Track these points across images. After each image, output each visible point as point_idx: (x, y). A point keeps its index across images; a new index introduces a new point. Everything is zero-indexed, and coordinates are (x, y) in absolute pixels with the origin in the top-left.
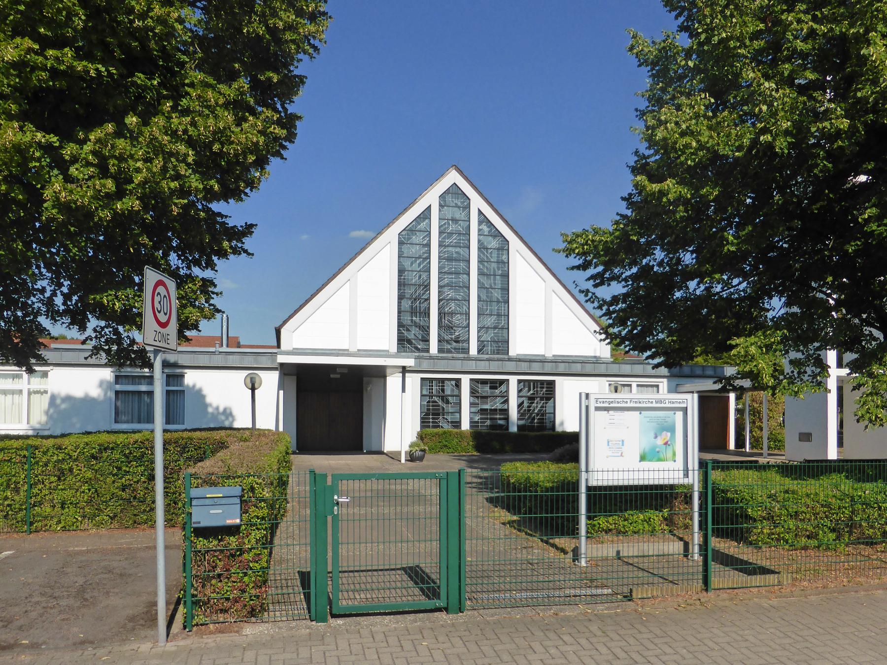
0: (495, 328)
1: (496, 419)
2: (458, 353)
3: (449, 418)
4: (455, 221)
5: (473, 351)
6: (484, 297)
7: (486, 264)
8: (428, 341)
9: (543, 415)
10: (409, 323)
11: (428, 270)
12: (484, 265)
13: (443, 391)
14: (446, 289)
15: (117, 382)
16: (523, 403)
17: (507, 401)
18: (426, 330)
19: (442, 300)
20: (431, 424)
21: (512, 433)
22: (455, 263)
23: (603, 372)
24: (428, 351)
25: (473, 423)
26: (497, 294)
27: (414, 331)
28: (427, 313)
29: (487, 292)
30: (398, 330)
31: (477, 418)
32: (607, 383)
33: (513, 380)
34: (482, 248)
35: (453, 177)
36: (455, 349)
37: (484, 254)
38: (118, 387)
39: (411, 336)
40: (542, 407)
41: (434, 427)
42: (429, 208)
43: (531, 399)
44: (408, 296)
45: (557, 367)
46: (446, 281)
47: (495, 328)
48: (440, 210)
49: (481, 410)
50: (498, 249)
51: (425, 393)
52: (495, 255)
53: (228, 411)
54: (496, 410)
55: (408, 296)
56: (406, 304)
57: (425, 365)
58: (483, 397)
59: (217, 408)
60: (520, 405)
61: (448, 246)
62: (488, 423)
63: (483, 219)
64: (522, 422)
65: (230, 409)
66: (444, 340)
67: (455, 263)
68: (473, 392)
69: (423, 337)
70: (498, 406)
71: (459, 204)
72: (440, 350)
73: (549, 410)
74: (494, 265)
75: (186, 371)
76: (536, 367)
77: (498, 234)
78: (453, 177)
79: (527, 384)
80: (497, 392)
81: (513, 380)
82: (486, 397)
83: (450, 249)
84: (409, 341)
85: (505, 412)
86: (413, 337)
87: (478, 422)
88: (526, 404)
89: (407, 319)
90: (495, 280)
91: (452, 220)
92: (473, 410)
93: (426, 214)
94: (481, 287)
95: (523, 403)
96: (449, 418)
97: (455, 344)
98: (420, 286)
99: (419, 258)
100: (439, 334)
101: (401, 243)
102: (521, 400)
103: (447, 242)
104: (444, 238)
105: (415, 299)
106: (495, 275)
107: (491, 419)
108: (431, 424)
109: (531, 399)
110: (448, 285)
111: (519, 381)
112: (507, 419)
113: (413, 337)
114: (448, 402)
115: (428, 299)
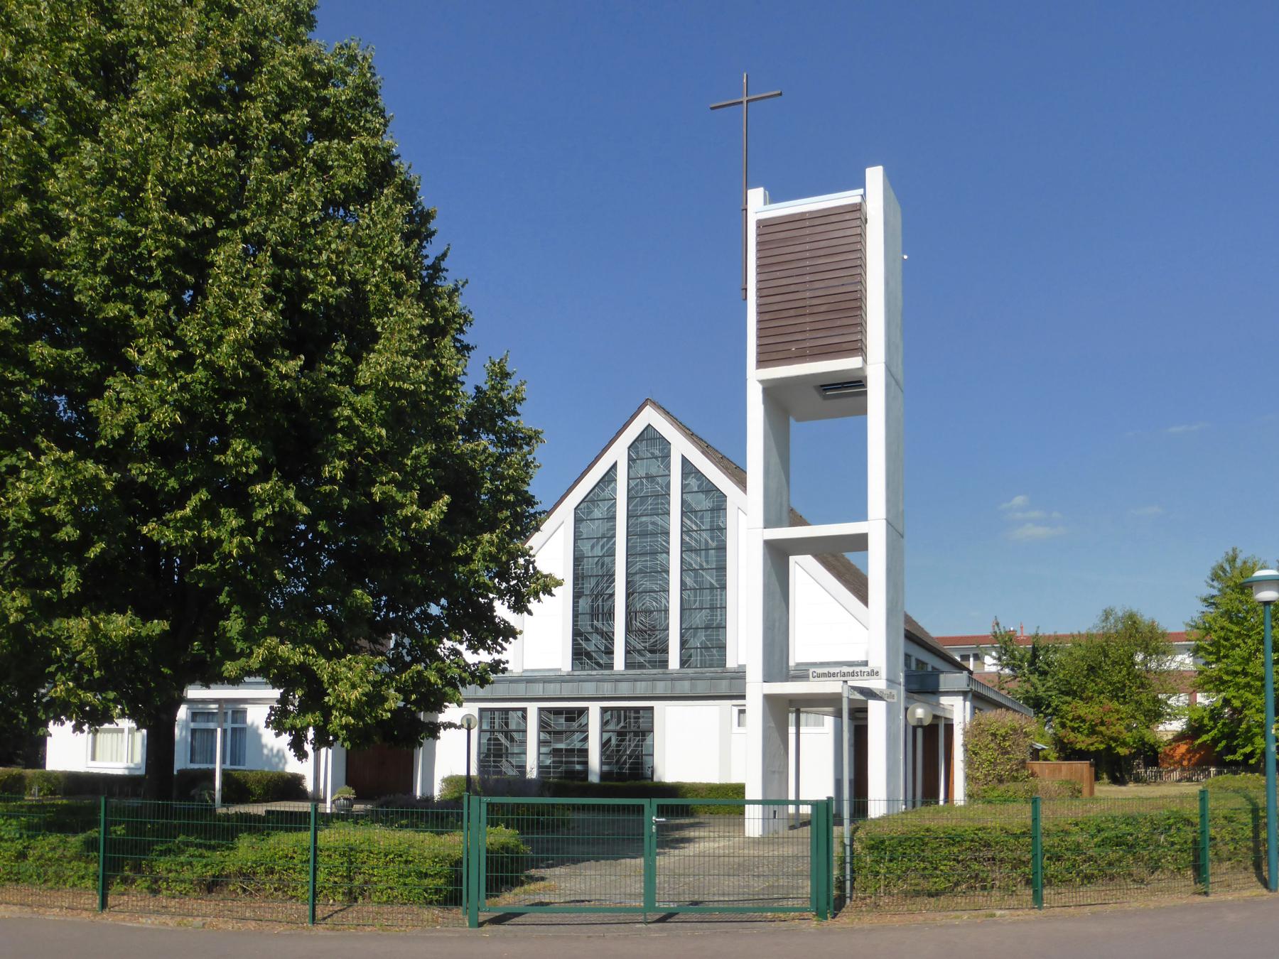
0: (707, 628)
1: (573, 763)
2: (654, 667)
4: (650, 478)
6: (689, 582)
7: (694, 534)
8: (612, 653)
9: (637, 757)
11: (612, 553)
12: (691, 537)
14: (637, 577)
15: (193, 720)
16: (609, 740)
17: (586, 739)
18: (609, 637)
21: (531, 781)
22: (647, 542)
23: (688, 692)
24: (611, 666)
25: (541, 767)
26: (710, 578)
27: (596, 639)
28: (610, 615)
30: (574, 640)
31: (548, 762)
33: (594, 709)
34: (686, 510)
35: (649, 416)
37: (691, 520)
38: (192, 725)
40: (636, 746)
41: (495, 773)
42: (614, 466)
43: (621, 734)
44: (587, 592)
45: (654, 688)
46: (638, 566)
47: (707, 628)
50: (712, 510)
51: (485, 727)
52: (707, 519)
54: (573, 750)
56: (584, 603)
57: (607, 689)
58: (557, 733)
59: (272, 750)
60: (605, 745)
61: (642, 515)
62: (563, 768)
63: (688, 468)
64: (606, 768)
66: (635, 650)
67: (647, 542)
68: (543, 726)
69: (606, 647)
70: (578, 745)
71: (657, 453)
72: (628, 665)
77: (710, 489)
78: (649, 416)
80: (575, 725)
81: (594, 709)
82: (560, 733)
83: (644, 519)
85: (584, 752)
86: (593, 648)
87: (548, 767)
88: (613, 742)
89: (586, 626)
90: (707, 556)
91: (647, 478)
92: (543, 750)
93: (609, 477)
95: (609, 740)
96: (514, 761)
97: (649, 655)
98: (603, 576)
100: (626, 642)
101: (578, 521)
102: (606, 736)
104: (636, 505)
106: (707, 549)
107: (567, 763)
109: (621, 734)
110: (641, 571)
111: (604, 710)
112: (586, 763)
113: (593, 648)
114: (512, 740)
115: (612, 595)
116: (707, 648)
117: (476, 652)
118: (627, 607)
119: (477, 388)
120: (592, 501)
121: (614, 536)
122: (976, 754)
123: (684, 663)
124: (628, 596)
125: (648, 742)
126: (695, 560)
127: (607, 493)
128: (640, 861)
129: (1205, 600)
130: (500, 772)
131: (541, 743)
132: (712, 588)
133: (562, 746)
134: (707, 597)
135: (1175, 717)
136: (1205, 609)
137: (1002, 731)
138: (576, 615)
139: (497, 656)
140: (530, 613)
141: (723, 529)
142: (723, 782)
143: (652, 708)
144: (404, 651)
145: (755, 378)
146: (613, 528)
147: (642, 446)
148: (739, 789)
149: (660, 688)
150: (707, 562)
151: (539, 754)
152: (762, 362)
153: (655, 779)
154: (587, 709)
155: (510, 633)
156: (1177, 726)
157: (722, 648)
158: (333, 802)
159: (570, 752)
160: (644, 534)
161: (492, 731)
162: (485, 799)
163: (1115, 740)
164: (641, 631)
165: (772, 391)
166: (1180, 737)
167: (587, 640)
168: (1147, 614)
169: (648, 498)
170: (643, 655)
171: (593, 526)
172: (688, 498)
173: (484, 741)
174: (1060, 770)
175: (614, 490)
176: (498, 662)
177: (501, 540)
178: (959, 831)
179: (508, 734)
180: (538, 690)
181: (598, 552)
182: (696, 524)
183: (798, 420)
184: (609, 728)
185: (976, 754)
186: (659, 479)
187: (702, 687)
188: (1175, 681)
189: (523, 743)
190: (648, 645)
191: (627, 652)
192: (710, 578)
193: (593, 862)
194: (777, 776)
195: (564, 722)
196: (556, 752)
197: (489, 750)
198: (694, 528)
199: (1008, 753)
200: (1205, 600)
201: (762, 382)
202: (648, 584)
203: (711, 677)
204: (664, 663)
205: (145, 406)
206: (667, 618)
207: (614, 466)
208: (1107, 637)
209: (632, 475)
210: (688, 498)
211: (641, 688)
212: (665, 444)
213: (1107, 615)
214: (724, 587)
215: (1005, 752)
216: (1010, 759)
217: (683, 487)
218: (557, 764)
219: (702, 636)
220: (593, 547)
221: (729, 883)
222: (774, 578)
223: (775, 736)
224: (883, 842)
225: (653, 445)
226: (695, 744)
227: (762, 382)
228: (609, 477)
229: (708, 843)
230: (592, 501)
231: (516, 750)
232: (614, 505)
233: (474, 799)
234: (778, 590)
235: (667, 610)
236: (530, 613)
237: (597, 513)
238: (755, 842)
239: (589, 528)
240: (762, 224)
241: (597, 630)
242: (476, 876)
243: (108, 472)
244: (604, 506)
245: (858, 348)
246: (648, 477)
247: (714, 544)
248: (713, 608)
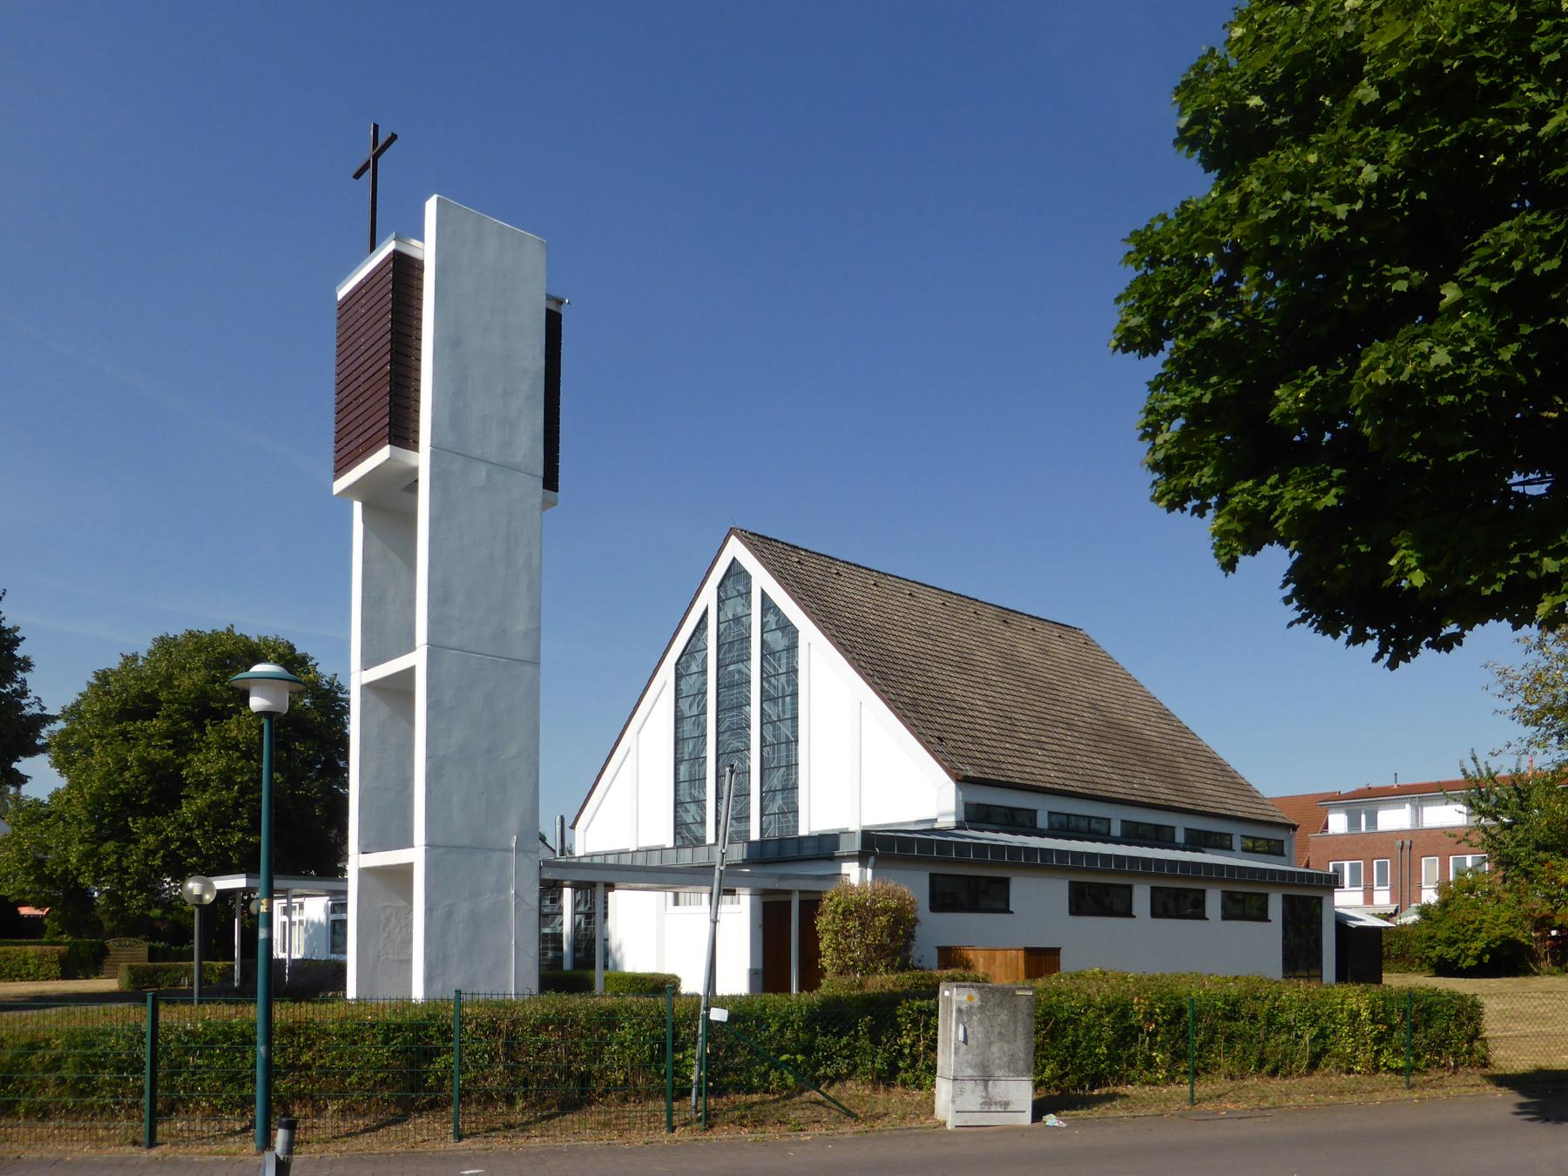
27: (693, 808)
47: (783, 790)
63: (767, 604)
101: (678, 677)
116: (784, 813)
121: (705, 693)
145: (418, 659)
146: (705, 683)
169: (733, 645)
205: (238, 743)
214: (797, 741)
223: (650, 986)
237: (694, 668)
239: (689, 685)
243: (1512, 214)
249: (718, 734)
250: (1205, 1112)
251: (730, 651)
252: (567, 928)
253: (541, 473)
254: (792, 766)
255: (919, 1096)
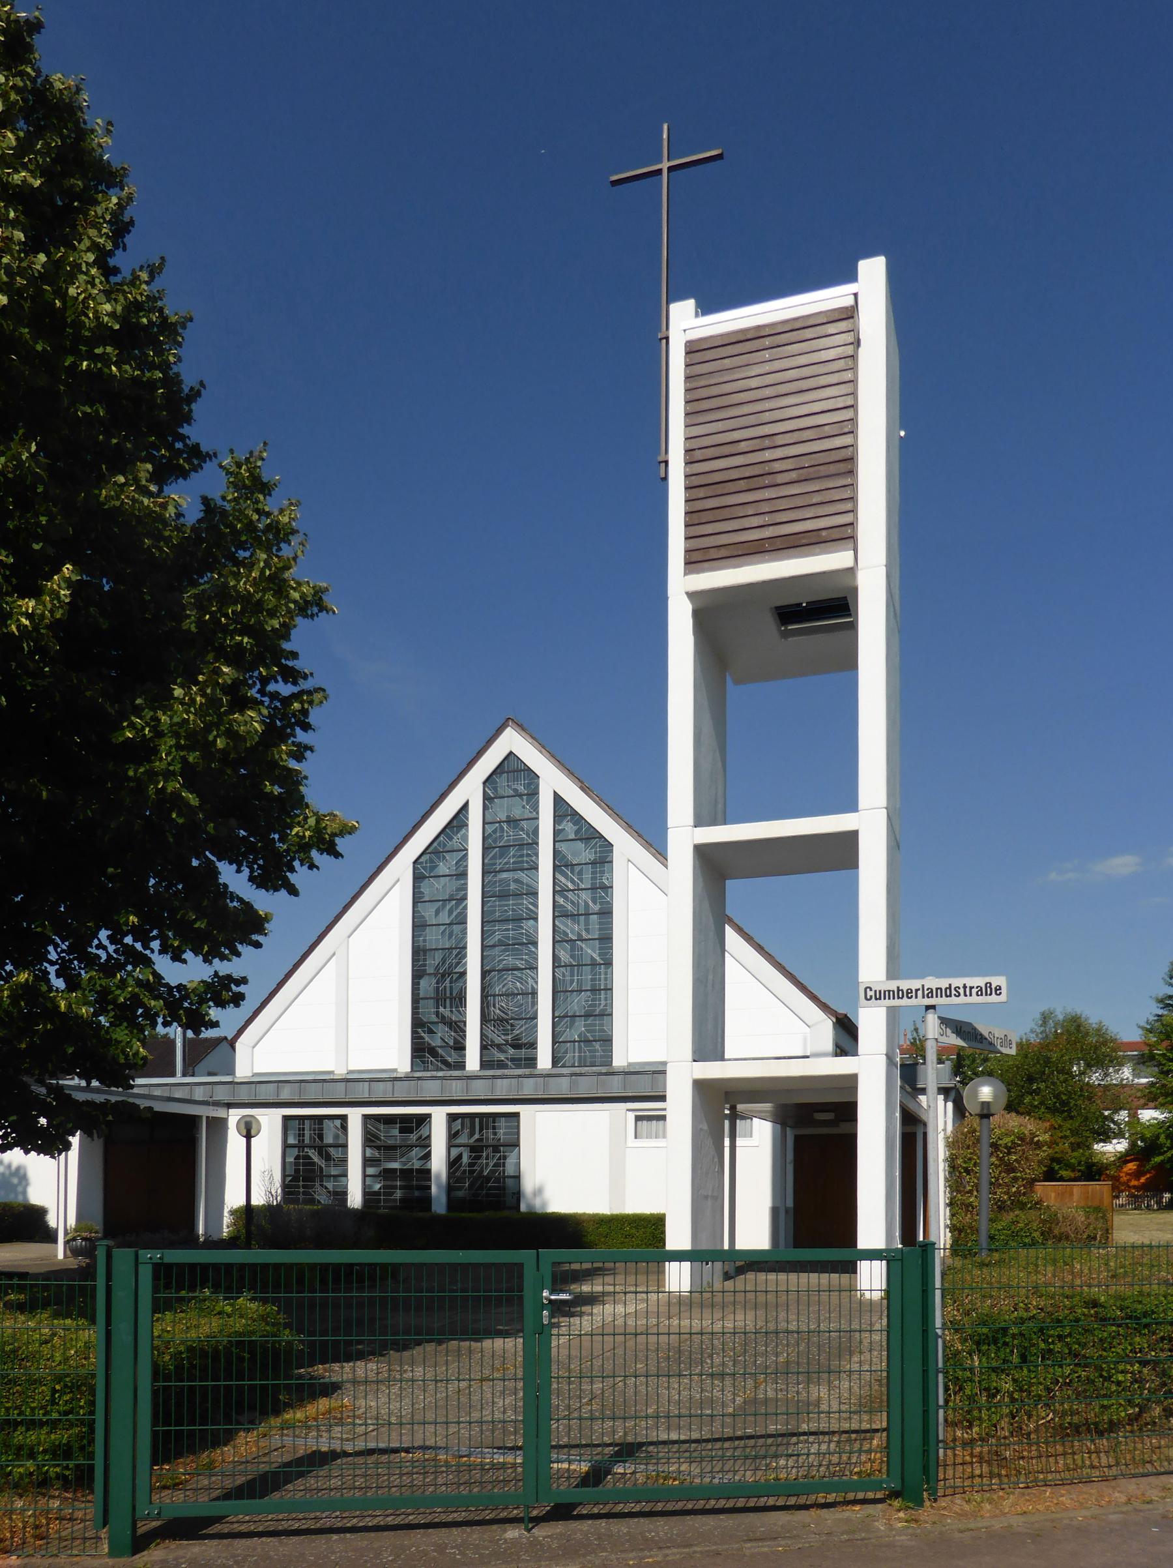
0: (587, 1016)
2: (518, 1067)
3: (330, 1185)
4: (512, 822)
5: (544, 1060)
7: (570, 895)
8: (464, 1048)
10: (434, 1018)
11: (462, 920)
12: (566, 898)
13: (321, 1137)
16: (460, 1157)
17: (428, 1156)
18: (459, 1028)
19: (490, 971)
20: (301, 1197)
21: (354, 1211)
24: (461, 1065)
25: (367, 1194)
26: (591, 952)
27: (442, 1031)
28: (460, 999)
29: (572, 949)
30: (414, 1032)
32: (631, 1116)
33: (439, 1117)
34: (561, 864)
35: (511, 741)
36: (512, 1060)
39: (436, 1042)
40: (496, 1165)
41: (306, 1202)
42: (465, 806)
44: (430, 970)
45: (519, 1087)
46: (497, 937)
47: (587, 1016)
48: (485, 808)
49: (387, 1171)
50: (594, 863)
52: (587, 876)
53: (22, 1172)
55: (430, 970)
56: (427, 985)
57: (456, 1089)
61: (499, 871)
65: (25, 1169)
68: (369, 1139)
70: (417, 1165)
71: (521, 789)
72: (484, 1064)
73: (510, 1170)
74: (585, 896)
75: (523, 1110)
76: (312, 1094)
77: (591, 836)
78: (511, 741)
79: (467, 1121)
80: (413, 1137)
81: (439, 1117)
83: (504, 875)
84: (433, 1051)
86: (439, 1042)
87: (377, 1193)
90: (587, 923)
92: (371, 1171)
93: (459, 821)
94: (559, 939)
95: (460, 1157)
96: (330, 1185)
97: (511, 1051)
99: (450, 900)
101: (418, 878)
102: (455, 1152)
103: (500, 863)
104: (494, 858)
105: (443, 975)
106: (587, 914)
108: (301, 1197)
110: (501, 943)
111: (452, 1118)
113: (439, 1042)
114: (328, 1158)
115: (464, 974)
117: (177, 957)
118: (483, 989)
119: (205, 501)
120: (436, 852)
121: (464, 898)
122: (968, 1171)
123: (555, 1061)
124: (484, 974)
125: (510, 1161)
126: (572, 929)
127: (455, 842)
128: (510, 1347)
129: (1161, 1001)
130: (312, 1201)
131: (367, 1162)
132: (594, 964)
133: (395, 1165)
134: (587, 975)
135: (1120, 1135)
136: (1160, 1012)
137: (1007, 1140)
138: (416, 1000)
139: (223, 968)
140: (293, 891)
141: (608, 888)
142: (616, 1211)
143: (516, 1115)
144: (52, 970)
145: (681, 586)
146: (464, 888)
147: (502, 781)
148: (653, 1227)
149: (529, 1088)
150: (587, 930)
151: (365, 1176)
152: (695, 561)
153: (523, 1208)
154: (429, 1116)
155: (249, 926)
156: (1119, 1146)
157: (608, 1041)
158: (66, 1243)
159: (406, 1174)
160: (504, 895)
161: (301, 1146)
162: (147, 1255)
163: (1058, 1161)
164: (502, 1020)
165: (710, 612)
166: (1123, 1158)
167: (431, 1032)
168: (1095, 1014)
169: (509, 849)
170: (505, 1052)
171: (438, 884)
172: (563, 847)
173: (290, 1159)
174: (1071, 1194)
175: (465, 838)
176: (227, 981)
177: (213, 702)
178: (1149, 1304)
179: (322, 1150)
180: (362, 1092)
181: (444, 918)
182: (573, 882)
183: (737, 682)
184: (460, 1141)
185: (968, 1171)
186: (524, 824)
187: (585, 1087)
188: (1117, 1097)
189: (344, 1161)
190: (509, 1044)
191: (484, 1048)
192: (591, 952)
193: (430, 1347)
194: (709, 1202)
195: (396, 1135)
196: (387, 1174)
197: (297, 1171)
198: (571, 886)
199: (1014, 1170)
200: (1161, 1001)
201: (691, 595)
202: (510, 961)
203: (593, 1072)
204: (532, 1061)
206: (535, 1003)
207: (465, 806)
208: (1045, 1046)
209: (489, 818)
210: (563, 847)
211: (503, 1088)
212: (532, 778)
213: (1045, 1018)
214: (609, 963)
215: (1010, 1169)
216: (1015, 1179)
217: (556, 833)
218: (388, 1190)
219: (580, 1026)
220: (437, 912)
221: (677, 1392)
222: (706, 905)
223: (709, 1142)
224: (1005, 1330)
225: (516, 779)
226: (570, 1162)
227: (691, 595)
228: (459, 821)
229: (617, 1308)
230: (436, 852)
231: (334, 1171)
232: (465, 857)
233: (123, 1256)
234: (712, 927)
235: (534, 993)
236: (293, 891)
237: (443, 868)
238: (682, 1303)
239: (436, 888)
240: (693, 349)
241: (443, 1020)
242: (131, 1422)
244: (452, 859)
245: (846, 536)
246: (510, 821)
247: (596, 908)
248: (595, 990)
249: (484, 947)
250: (21, 1289)
251: (502, 856)
252: (438, 1162)
253: (884, 562)
254: (602, 990)
255: (845, 1277)
